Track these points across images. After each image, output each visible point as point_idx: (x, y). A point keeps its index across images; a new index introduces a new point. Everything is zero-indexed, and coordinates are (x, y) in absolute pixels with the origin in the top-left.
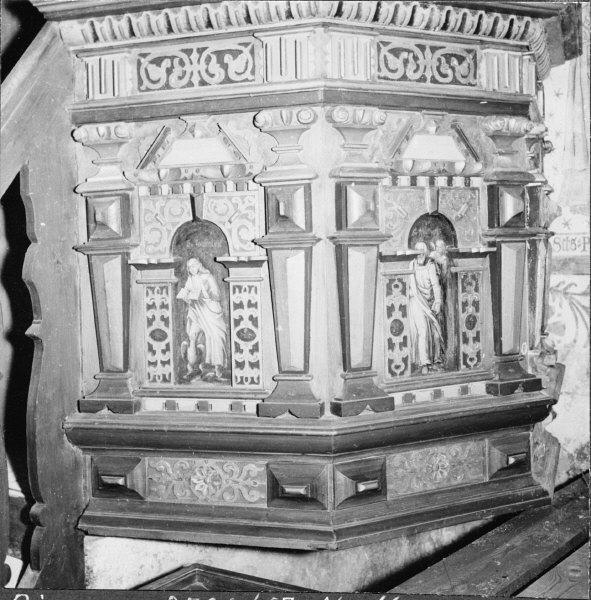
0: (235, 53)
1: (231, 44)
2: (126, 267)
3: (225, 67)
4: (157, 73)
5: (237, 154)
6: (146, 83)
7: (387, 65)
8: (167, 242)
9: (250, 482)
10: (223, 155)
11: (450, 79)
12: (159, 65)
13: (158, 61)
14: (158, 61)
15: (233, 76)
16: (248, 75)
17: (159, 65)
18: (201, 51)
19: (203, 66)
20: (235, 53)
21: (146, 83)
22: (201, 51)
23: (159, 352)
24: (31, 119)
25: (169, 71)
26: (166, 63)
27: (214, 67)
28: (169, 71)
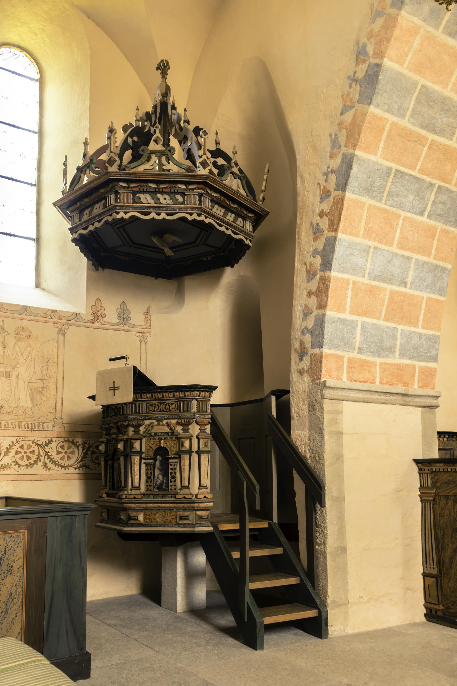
0: (172, 404)
1: (172, 401)
2: (141, 459)
3: (170, 406)
4: (152, 408)
5: (171, 429)
6: (148, 410)
7: (149, 409)
8: (152, 453)
9: (173, 517)
10: (167, 429)
11: (168, 410)
12: (152, 406)
13: (152, 405)
14: (152, 405)
15: (171, 409)
16: (176, 409)
17: (152, 406)
18: (164, 403)
19: (164, 407)
20: (172, 404)
21: (148, 410)
22: (164, 403)
23: (149, 473)
24: (370, 329)
25: (155, 407)
26: (154, 406)
27: (167, 407)
28: (155, 407)
